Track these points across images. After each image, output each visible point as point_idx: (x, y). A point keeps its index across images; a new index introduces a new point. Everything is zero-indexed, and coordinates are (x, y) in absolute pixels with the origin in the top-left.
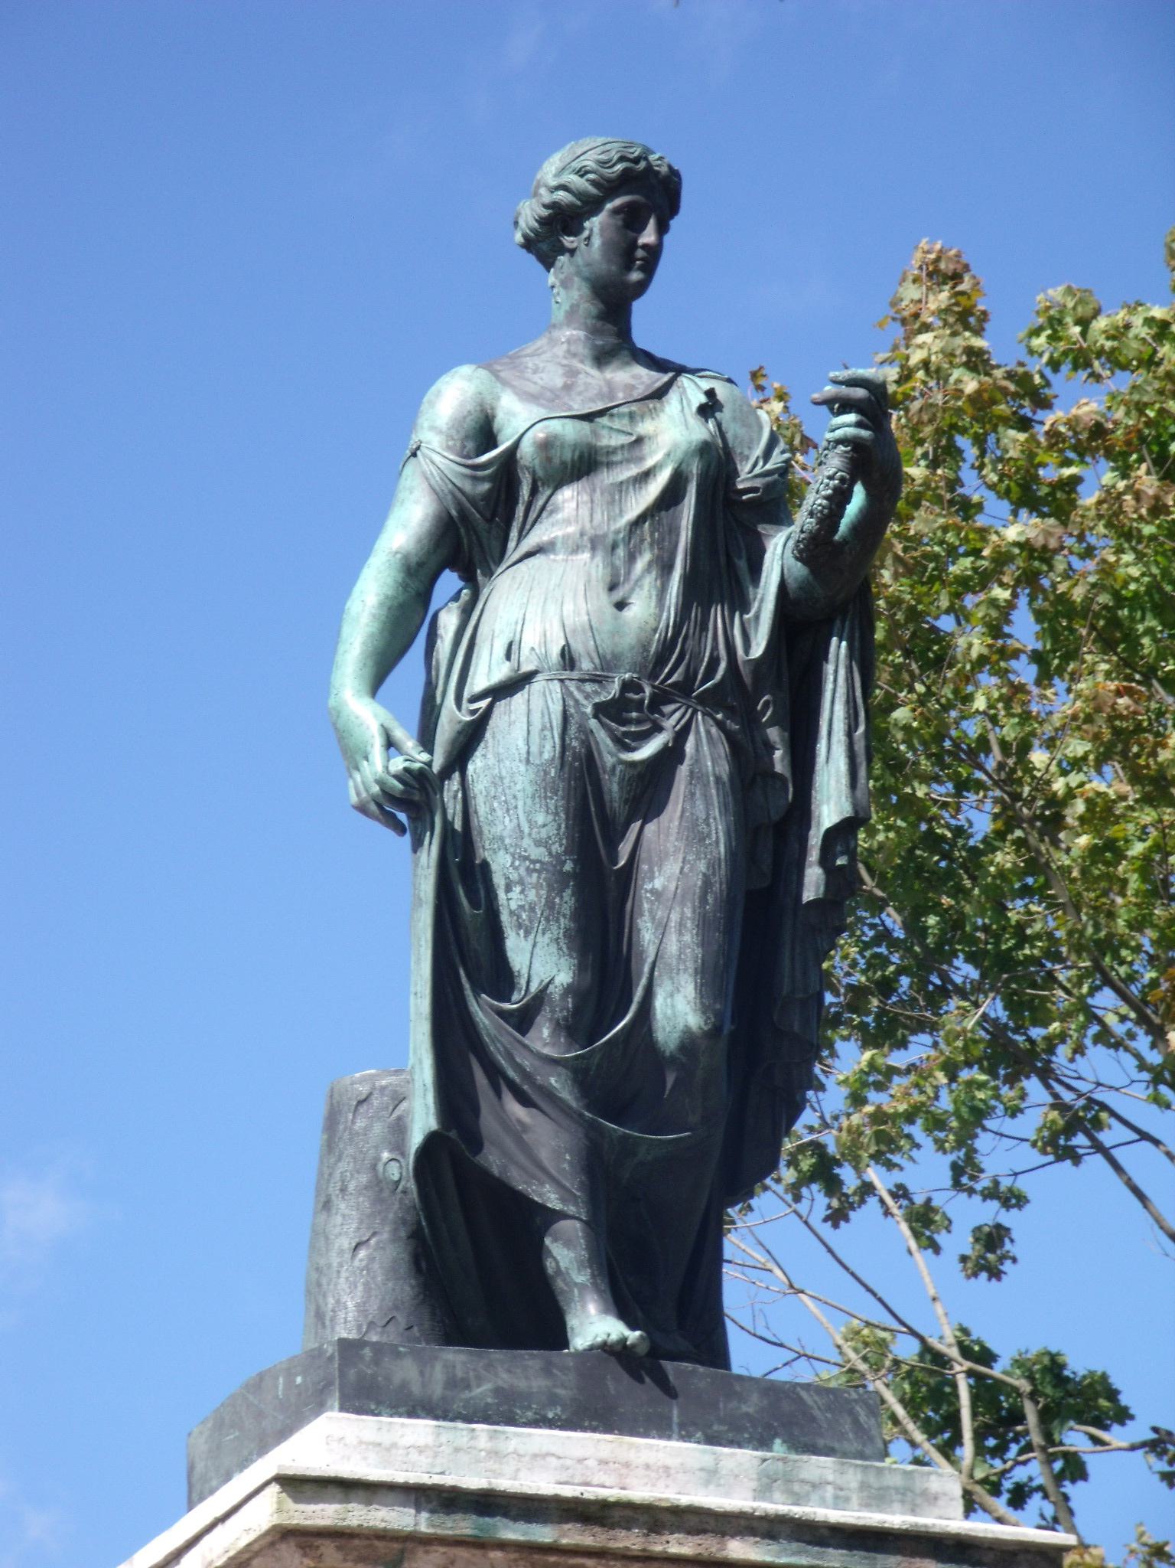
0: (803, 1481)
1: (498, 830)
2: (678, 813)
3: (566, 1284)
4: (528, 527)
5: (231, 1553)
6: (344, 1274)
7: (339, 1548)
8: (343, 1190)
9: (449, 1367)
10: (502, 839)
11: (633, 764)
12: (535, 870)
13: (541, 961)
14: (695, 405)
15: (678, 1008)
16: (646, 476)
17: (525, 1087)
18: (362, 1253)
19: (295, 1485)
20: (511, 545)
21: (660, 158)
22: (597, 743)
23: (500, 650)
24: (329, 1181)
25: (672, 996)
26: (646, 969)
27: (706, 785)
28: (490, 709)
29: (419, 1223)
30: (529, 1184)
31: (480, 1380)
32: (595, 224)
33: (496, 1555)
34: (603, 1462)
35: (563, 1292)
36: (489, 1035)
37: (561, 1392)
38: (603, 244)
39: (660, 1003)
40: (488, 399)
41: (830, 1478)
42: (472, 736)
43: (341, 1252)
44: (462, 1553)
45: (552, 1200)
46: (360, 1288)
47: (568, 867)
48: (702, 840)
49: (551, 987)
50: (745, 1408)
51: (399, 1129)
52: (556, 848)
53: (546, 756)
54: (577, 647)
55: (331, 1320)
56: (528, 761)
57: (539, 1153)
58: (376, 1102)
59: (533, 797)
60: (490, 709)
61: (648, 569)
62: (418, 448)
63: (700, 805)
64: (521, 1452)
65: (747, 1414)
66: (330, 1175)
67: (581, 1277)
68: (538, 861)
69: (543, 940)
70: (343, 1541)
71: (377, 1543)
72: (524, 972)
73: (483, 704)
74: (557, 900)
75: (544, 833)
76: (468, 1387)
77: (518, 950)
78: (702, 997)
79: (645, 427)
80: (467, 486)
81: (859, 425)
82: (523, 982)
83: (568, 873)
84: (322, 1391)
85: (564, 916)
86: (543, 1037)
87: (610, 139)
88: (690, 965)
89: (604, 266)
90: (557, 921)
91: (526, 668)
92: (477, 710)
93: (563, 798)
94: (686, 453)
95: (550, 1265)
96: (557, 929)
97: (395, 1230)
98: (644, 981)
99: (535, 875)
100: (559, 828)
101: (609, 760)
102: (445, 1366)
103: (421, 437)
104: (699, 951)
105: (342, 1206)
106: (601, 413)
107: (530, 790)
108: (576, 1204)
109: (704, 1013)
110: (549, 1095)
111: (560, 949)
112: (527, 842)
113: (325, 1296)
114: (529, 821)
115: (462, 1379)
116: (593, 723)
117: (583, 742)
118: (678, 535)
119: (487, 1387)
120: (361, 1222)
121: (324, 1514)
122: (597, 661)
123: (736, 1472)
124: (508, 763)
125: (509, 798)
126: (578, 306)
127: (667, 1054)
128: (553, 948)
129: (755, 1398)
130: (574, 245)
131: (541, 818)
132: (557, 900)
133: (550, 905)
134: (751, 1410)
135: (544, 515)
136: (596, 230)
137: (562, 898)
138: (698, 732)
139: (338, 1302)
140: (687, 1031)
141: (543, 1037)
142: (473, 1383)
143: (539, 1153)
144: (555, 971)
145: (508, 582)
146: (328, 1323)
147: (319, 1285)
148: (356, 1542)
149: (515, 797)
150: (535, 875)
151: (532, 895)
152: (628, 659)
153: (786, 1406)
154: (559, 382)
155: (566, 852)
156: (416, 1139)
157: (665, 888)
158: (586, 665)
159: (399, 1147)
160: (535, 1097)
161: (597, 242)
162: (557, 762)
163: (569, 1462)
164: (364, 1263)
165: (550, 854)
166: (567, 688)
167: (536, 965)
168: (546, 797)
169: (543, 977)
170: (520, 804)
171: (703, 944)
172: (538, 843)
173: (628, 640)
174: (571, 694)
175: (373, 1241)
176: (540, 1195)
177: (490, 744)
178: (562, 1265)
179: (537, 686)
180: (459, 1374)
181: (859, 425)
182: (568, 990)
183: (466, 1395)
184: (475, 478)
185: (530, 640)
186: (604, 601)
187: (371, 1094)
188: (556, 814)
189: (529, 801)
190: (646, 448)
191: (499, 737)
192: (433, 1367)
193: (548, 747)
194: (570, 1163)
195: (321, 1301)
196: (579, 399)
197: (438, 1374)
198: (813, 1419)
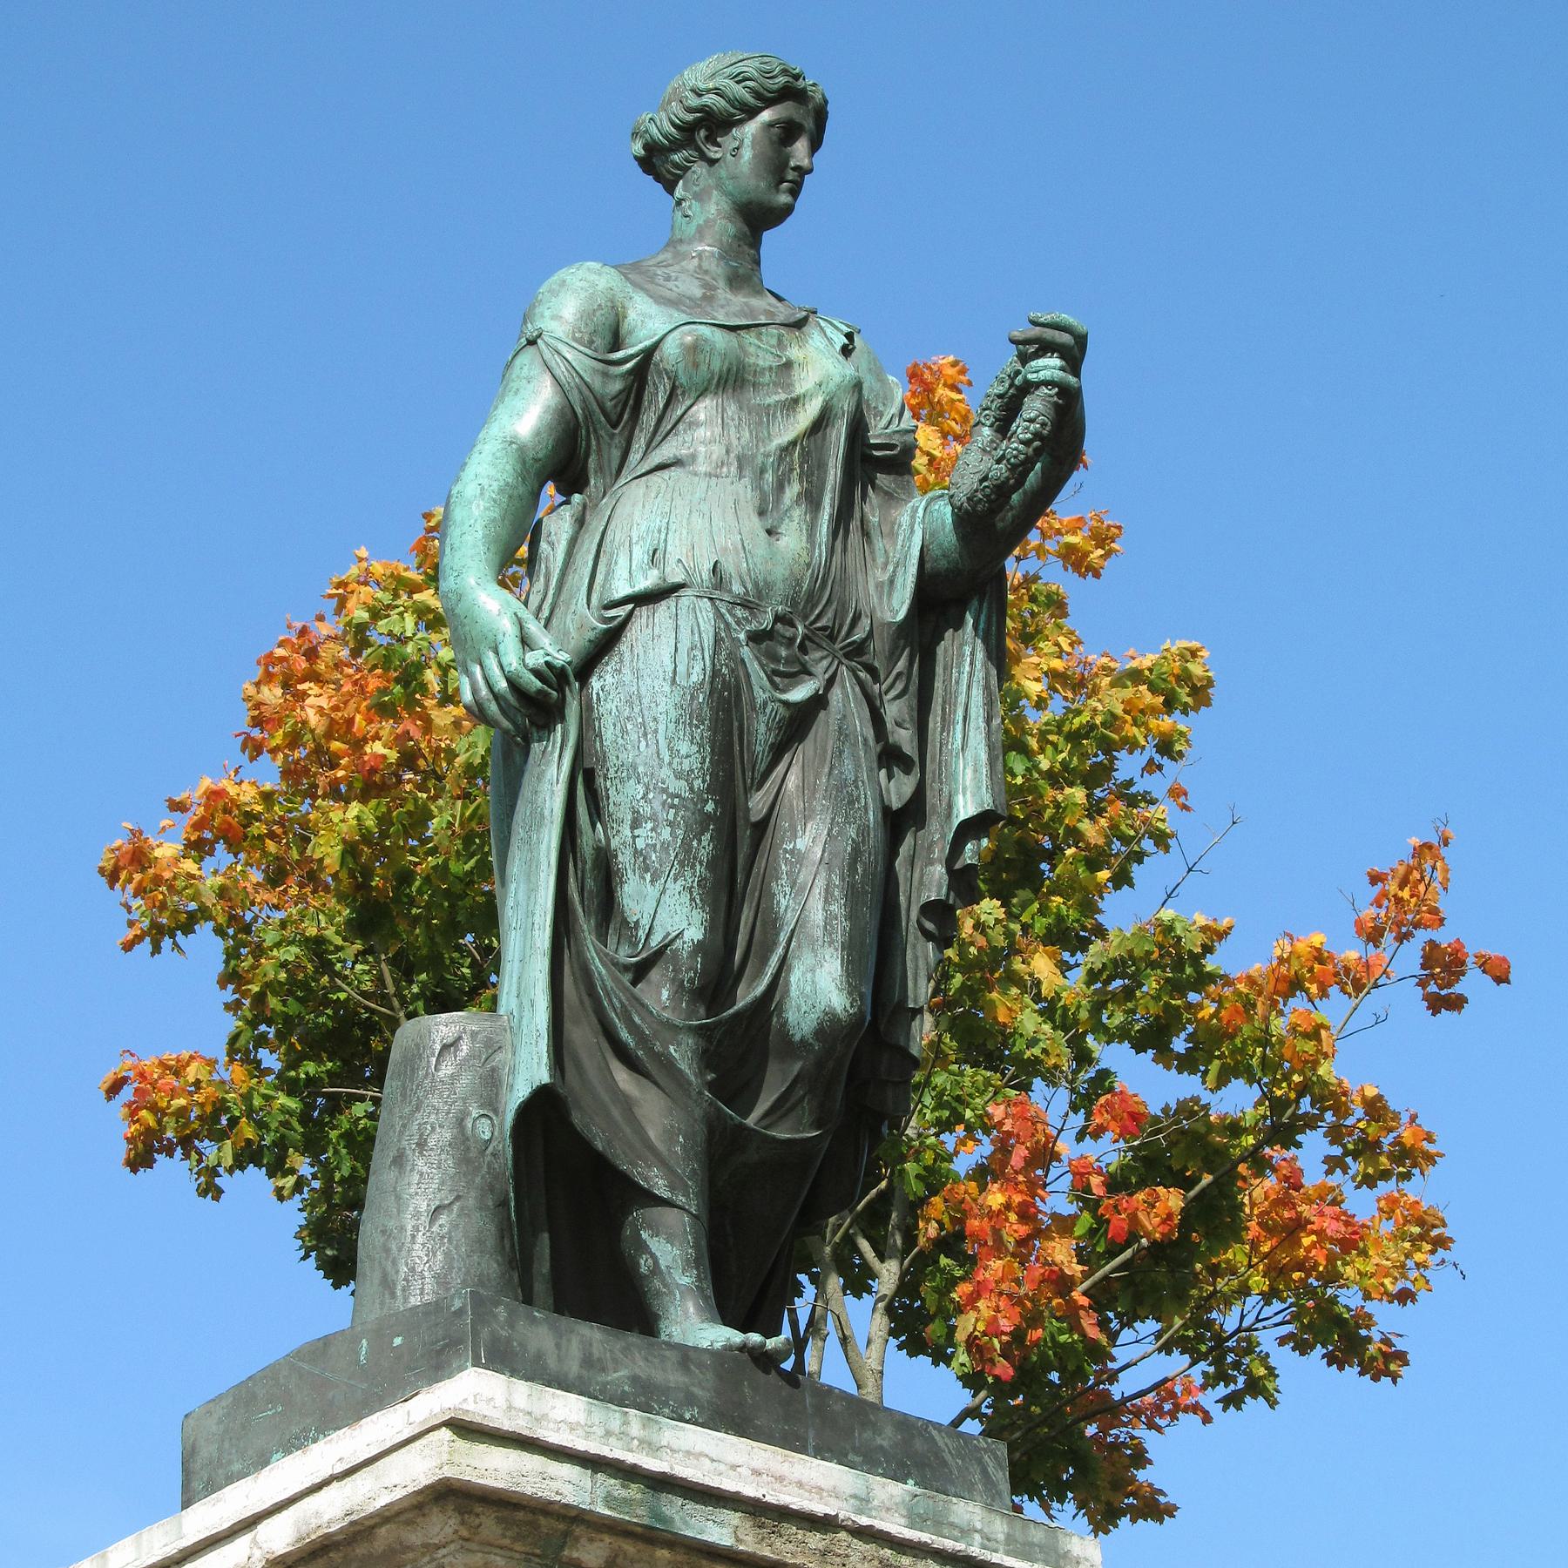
0: (952, 1525)
1: (628, 757)
2: (826, 770)
3: (665, 1286)
4: (658, 438)
5: (355, 1517)
6: (420, 1239)
7: (499, 1520)
8: (422, 1145)
9: (586, 1345)
10: (634, 766)
11: (786, 703)
12: (672, 806)
13: (667, 910)
14: (838, 348)
15: (819, 985)
16: (794, 403)
17: (640, 1053)
18: (443, 1219)
19: (465, 1429)
20: (634, 457)
21: (814, 85)
22: (748, 676)
23: (640, 554)
24: (401, 1133)
25: (813, 971)
26: (783, 938)
27: (855, 745)
28: (630, 615)
29: (507, 1194)
30: (635, 1165)
31: (617, 1364)
32: (751, 128)
33: (663, 1553)
34: (757, 1473)
35: (658, 1294)
36: (604, 988)
37: (696, 1391)
38: (754, 157)
39: (797, 978)
40: (620, 296)
41: (978, 1526)
42: (606, 643)
43: (417, 1215)
44: (629, 1547)
45: (661, 1188)
46: (440, 1256)
47: (710, 807)
48: (851, 803)
49: (678, 943)
50: (879, 1441)
51: (491, 1085)
52: (697, 783)
53: (694, 678)
54: (728, 566)
55: (404, 1290)
56: (673, 681)
57: (652, 1131)
58: (465, 1048)
59: (677, 722)
60: (630, 615)
61: (797, 502)
62: (539, 336)
63: (848, 765)
64: (675, 1447)
65: (881, 1447)
66: (404, 1126)
67: (685, 1279)
68: (678, 796)
69: (675, 887)
70: (506, 1513)
71: (542, 1520)
72: (645, 922)
73: (622, 612)
74: (695, 843)
75: (686, 765)
76: (603, 1370)
77: (636, 897)
78: (848, 976)
79: (794, 353)
80: (597, 383)
81: (1062, 369)
82: (642, 934)
83: (708, 815)
84: (440, 1352)
85: (701, 863)
86: (660, 995)
87: (746, 55)
88: (839, 937)
89: (753, 182)
90: (693, 867)
91: (677, 577)
92: (614, 618)
93: (710, 729)
94: (839, 386)
95: (644, 1265)
96: (690, 878)
97: (481, 1199)
98: (780, 951)
99: (672, 811)
100: (703, 763)
101: (760, 696)
102: (581, 1342)
103: (539, 325)
104: (847, 924)
105: (420, 1163)
106: (748, 327)
107: (673, 714)
108: (686, 1195)
109: (850, 993)
110: (668, 1065)
111: (692, 899)
112: (665, 773)
113: (394, 1263)
114: (671, 749)
115: (599, 1360)
116: (746, 652)
117: (732, 671)
118: (826, 472)
119: (623, 1373)
120: (442, 1183)
121: (496, 1468)
122: (750, 586)
123: (888, 1504)
124: (649, 681)
125: (649, 720)
126: (715, 221)
127: (797, 1038)
128: (686, 898)
129: (889, 1431)
130: (718, 156)
131: (684, 747)
132: (695, 843)
133: (686, 847)
134: (885, 1443)
135: (681, 427)
136: (747, 142)
137: (700, 841)
138: (844, 687)
139: (413, 1270)
140: (830, 1016)
141: (660, 995)
142: (610, 1365)
143: (652, 1131)
144: (684, 925)
145: (642, 491)
146: (399, 1293)
147: (387, 1250)
148: (520, 1515)
149: (655, 719)
150: (672, 811)
151: (666, 833)
152: (780, 589)
153: (919, 1445)
154: (698, 292)
155: (709, 790)
156: (520, 1091)
157: (808, 850)
158: (737, 588)
159: (492, 1104)
160: (650, 1066)
161: (747, 154)
162: (707, 687)
163: (722, 1467)
164: (445, 1230)
165: (691, 789)
166: (717, 609)
167: (662, 915)
168: (691, 724)
169: (670, 929)
170: (662, 728)
171: (851, 916)
172: (678, 775)
173: (779, 573)
174: (722, 615)
175: (455, 1207)
176: (646, 1179)
177: (627, 655)
178: (663, 1263)
179: (686, 599)
180: (596, 1354)
181: (1062, 369)
182: (699, 947)
183: (602, 1378)
184: (605, 375)
185: (676, 549)
186: (754, 524)
187: (460, 1038)
188: (700, 746)
189: (672, 726)
190: (796, 371)
191: (639, 649)
192: (569, 1341)
193: (698, 668)
194: (684, 1147)
195: (389, 1268)
196: (722, 311)
197: (575, 1350)
198: (944, 1463)
